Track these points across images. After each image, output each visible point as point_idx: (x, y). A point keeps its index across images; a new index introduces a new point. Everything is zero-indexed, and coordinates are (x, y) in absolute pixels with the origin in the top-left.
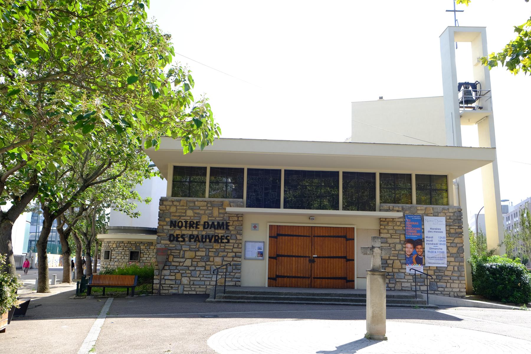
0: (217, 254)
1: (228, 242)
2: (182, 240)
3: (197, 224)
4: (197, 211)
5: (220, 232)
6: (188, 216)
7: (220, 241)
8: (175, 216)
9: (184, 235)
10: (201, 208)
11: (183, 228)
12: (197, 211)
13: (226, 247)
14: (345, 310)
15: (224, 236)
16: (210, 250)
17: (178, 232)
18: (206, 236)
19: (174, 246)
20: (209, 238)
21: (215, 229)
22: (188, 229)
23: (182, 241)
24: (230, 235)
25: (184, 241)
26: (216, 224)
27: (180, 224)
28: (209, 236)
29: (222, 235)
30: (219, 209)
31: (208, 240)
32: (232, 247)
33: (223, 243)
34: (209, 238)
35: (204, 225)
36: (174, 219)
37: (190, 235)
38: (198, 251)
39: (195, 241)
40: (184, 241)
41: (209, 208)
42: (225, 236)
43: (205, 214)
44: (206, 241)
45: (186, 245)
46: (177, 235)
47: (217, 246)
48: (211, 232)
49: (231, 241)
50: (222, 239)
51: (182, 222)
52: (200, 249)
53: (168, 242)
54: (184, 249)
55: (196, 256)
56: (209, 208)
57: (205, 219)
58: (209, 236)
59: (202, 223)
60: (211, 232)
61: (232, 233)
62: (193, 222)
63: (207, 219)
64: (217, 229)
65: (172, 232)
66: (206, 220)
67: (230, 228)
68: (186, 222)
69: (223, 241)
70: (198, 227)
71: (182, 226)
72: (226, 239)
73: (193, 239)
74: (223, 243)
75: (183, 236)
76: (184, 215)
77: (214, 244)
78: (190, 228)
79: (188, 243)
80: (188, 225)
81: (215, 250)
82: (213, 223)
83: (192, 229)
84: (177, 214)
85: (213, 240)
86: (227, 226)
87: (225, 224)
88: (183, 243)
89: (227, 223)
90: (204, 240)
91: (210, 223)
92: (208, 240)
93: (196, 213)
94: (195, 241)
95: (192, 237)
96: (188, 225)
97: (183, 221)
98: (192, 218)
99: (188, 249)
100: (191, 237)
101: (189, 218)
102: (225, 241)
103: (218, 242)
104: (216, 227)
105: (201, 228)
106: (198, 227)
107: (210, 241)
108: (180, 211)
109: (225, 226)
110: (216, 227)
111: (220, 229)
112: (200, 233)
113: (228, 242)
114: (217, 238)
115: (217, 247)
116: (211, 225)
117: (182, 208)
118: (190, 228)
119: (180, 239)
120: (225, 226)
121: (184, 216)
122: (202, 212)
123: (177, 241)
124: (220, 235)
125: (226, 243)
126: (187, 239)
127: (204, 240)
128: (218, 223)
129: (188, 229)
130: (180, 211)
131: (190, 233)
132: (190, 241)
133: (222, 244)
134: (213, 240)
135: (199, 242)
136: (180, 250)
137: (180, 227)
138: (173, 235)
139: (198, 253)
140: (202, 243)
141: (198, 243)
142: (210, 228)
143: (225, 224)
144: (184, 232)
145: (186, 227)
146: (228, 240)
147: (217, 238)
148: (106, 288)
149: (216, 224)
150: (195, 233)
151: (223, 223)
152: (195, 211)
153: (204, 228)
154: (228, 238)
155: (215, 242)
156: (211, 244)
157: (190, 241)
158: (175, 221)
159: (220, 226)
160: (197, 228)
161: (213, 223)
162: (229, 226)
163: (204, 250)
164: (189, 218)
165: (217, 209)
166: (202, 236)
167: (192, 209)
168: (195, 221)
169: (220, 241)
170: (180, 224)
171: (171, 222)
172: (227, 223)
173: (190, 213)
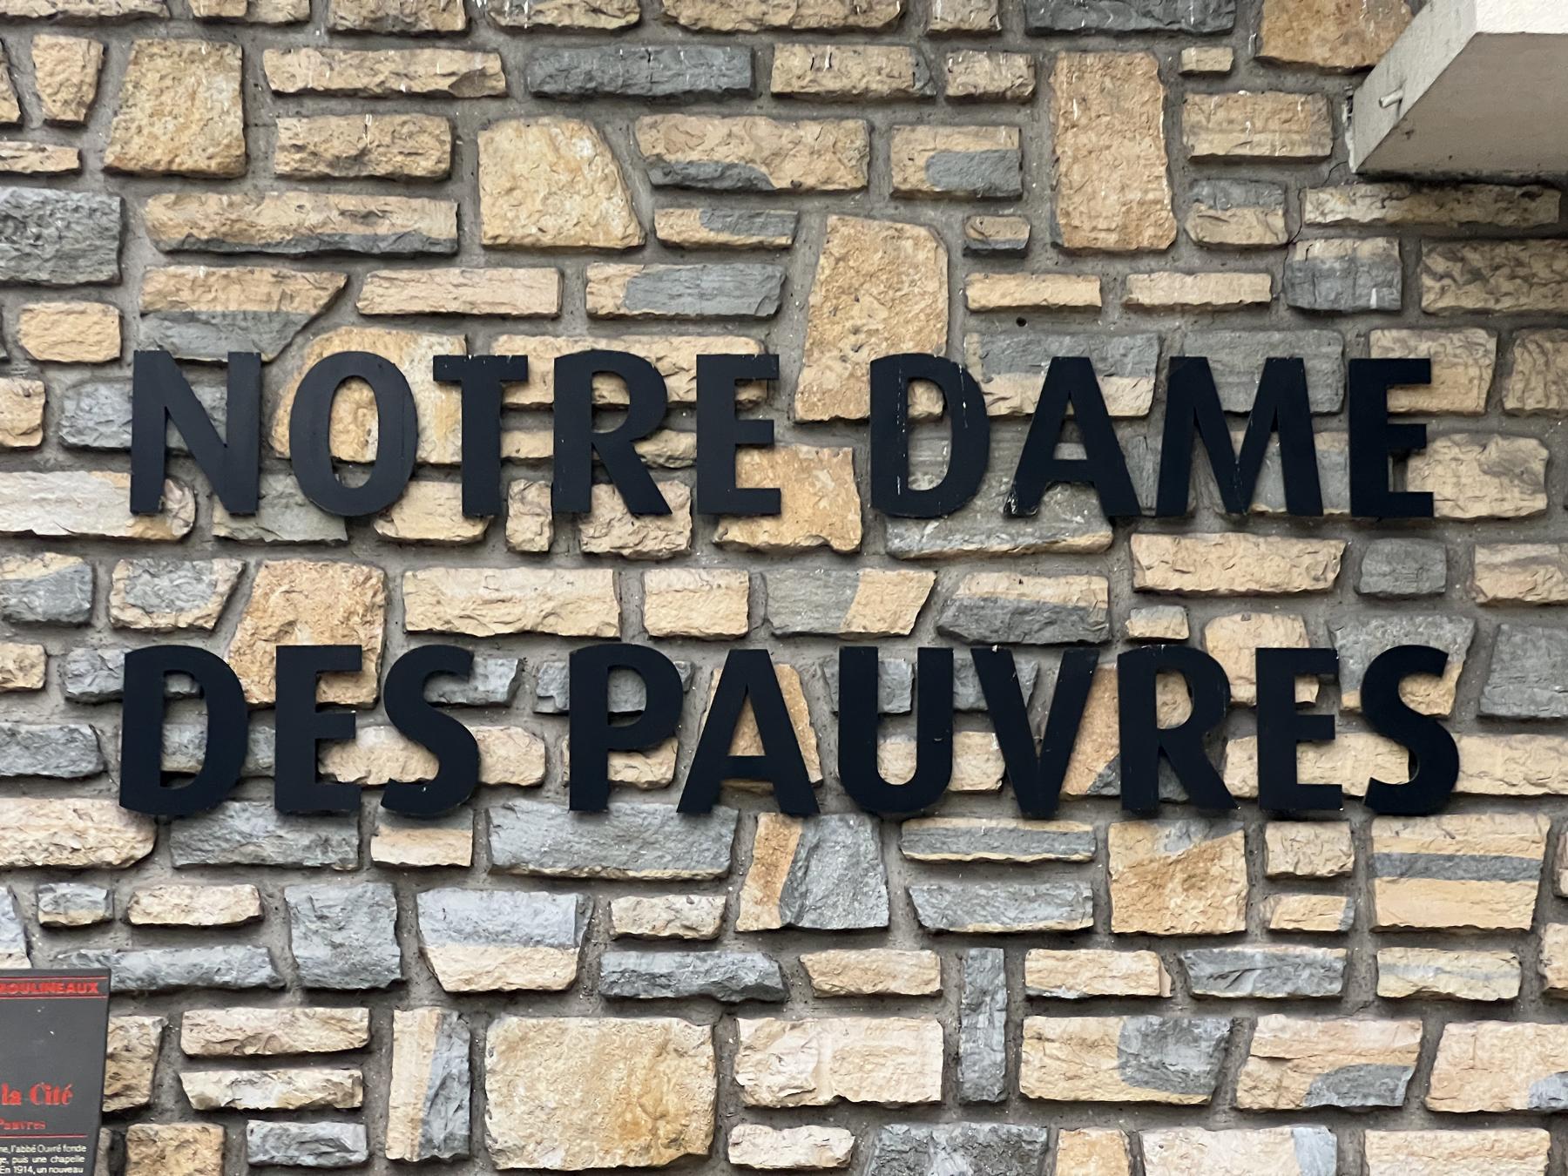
0: (1192, 1060)
1: (1432, 787)
2: (417, 766)
3: (739, 401)
4: (710, 142)
5: (1237, 584)
6: (508, 252)
7: (1240, 768)
8: (223, 252)
9: (448, 654)
10: (792, 66)
11: (433, 510)
12: (710, 142)
13: (1397, 903)
14: (260, 999)
15: (1321, 663)
16: (1045, 970)
17: (317, 599)
18: (934, 671)
19: (228, 901)
20: (1004, 712)
21: (1123, 515)
22: (528, 519)
23: (410, 805)
24: (1448, 634)
25: (456, 790)
26: (1128, 395)
27: (354, 430)
28: (995, 663)
29: (1282, 632)
30: (1182, 84)
31: (978, 760)
32: (1512, 905)
33: (1323, 804)
34: (1012, 698)
35: (883, 434)
36: (228, 306)
37: (595, 660)
38: (765, 1001)
39: (698, 801)
40: (456, 790)
41: (976, 72)
42: (1361, 643)
43: (879, 194)
44: (932, 789)
45: (508, 875)
46: (302, 667)
47: (1174, 875)
48: (1032, 579)
49: (1484, 762)
50: (1287, 728)
51: (385, 380)
52: (832, 968)
53: (100, 826)
54: (458, 965)
55: (731, 1105)
56: (976, 72)
57: (873, 299)
58: (995, 663)
59: (830, 381)
60: (1032, 579)
61: (1500, 573)
62: (643, 377)
63: (929, 291)
64: (1175, 515)
65: (180, 597)
66: (917, 334)
67: (1451, 477)
68: (484, 385)
69: (1312, 767)
70: (754, 470)
71: (401, 464)
72: (1384, 714)
73: (646, 734)
74: (1323, 804)
75: (427, 682)
76: (431, 220)
77: (1132, 846)
78: (570, 511)
79: (536, 829)
80: (530, 443)
81: (1137, 972)
82: (1072, 385)
83: (610, 520)
84: (281, 214)
85: (1095, 757)
86: (1386, 441)
87: (1325, 392)
88: (444, 845)
89: (1370, 380)
90: (897, 759)
91: (1013, 391)
92: (978, 760)
93: (680, 188)
94: (698, 801)
95: (628, 696)
96: (530, 443)
97: (416, 358)
98: (609, 287)
99: (556, 971)
100: (613, 698)
101: (531, 289)
102: (1359, 760)
103: (1213, 805)
104: (1144, 461)
105: (818, 491)
106: (754, 470)
107: (1035, 786)
108: (338, 135)
109: (1332, 447)
110: (1144, 461)
111: (1240, 514)
112: (800, 599)
113: (1432, 787)
114: (1174, 706)
115: (1185, 913)
116: (1044, 424)
117: (386, 67)
118: (570, 511)
119: (379, 755)
120: (1332, 447)
121: (425, 257)
122: (808, 153)
123: (311, 798)
124: (1235, 645)
125: (1384, 801)
126: (510, 750)
127: (897, 759)
128: (1187, 384)
129: (528, 519)
130: (338, 135)
131: (584, 603)
132: (590, 794)
133: (1298, 846)
134: (1095, 757)
135: (799, 802)
136: (384, 995)
137: (356, 511)
138: (217, 684)
139: (792, 1055)
140: (847, 836)
141: (770, 831)
142: (1024, 505)
143: (1325, 392)
144: (446, 598)
145: (485, 497)
146: (1432, 750)
147: (1174, 706)
148: (1392, 297)
149: (1128, 395)
150: (695, 602)
151: (1284, 379)
152: (658, 136)
153: (889, 497)
154: (1426, 697)
155: (1137, 800)
156: (1069, 835)
157: (590, 794)
158: (247, 374)
159: (1211, 446)
160: (723, 499)
161: (1072, 385)
162: (1413, 438)
163: (908, 967)
164: (531, 289)
165: (1145, 97)
166: (858, 662)
167: (582, 101)
168: (677, 358)
169: (1240, 768)
170: (354, 430)
171: (158, 380)
172: (1370, 380)
173: (548, 177)
